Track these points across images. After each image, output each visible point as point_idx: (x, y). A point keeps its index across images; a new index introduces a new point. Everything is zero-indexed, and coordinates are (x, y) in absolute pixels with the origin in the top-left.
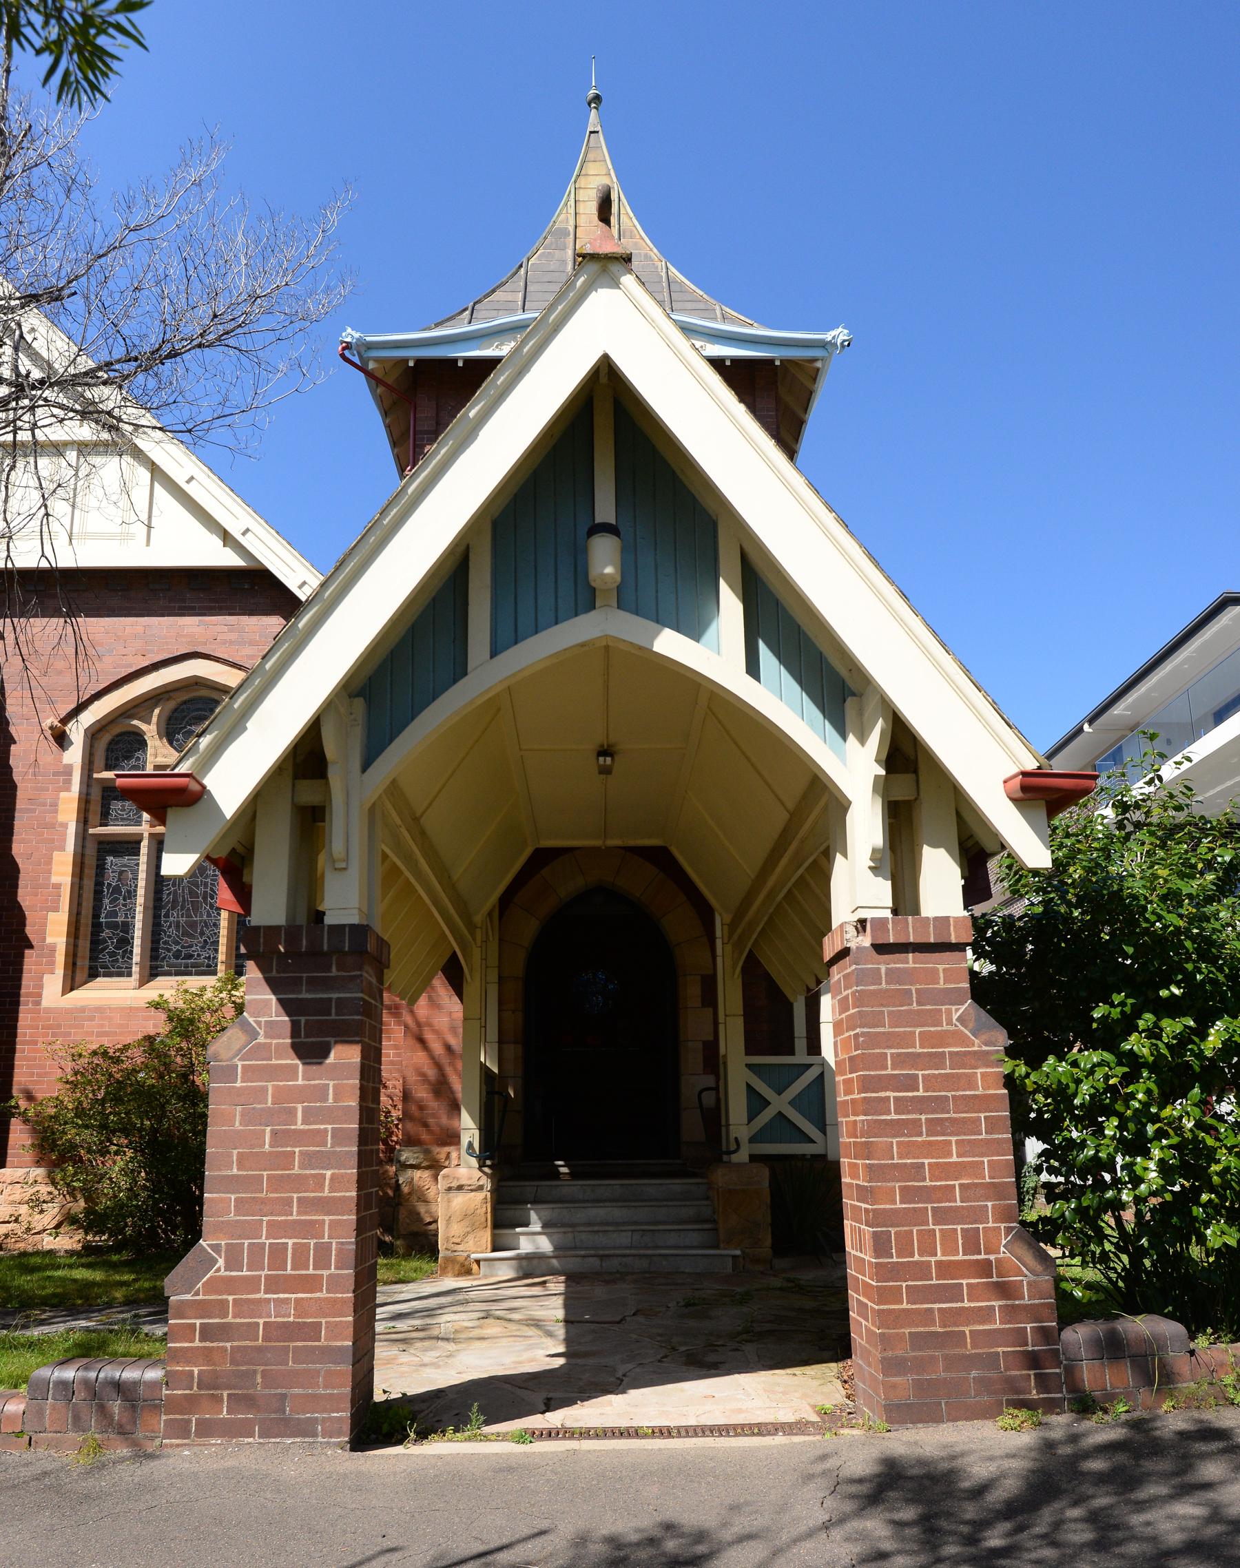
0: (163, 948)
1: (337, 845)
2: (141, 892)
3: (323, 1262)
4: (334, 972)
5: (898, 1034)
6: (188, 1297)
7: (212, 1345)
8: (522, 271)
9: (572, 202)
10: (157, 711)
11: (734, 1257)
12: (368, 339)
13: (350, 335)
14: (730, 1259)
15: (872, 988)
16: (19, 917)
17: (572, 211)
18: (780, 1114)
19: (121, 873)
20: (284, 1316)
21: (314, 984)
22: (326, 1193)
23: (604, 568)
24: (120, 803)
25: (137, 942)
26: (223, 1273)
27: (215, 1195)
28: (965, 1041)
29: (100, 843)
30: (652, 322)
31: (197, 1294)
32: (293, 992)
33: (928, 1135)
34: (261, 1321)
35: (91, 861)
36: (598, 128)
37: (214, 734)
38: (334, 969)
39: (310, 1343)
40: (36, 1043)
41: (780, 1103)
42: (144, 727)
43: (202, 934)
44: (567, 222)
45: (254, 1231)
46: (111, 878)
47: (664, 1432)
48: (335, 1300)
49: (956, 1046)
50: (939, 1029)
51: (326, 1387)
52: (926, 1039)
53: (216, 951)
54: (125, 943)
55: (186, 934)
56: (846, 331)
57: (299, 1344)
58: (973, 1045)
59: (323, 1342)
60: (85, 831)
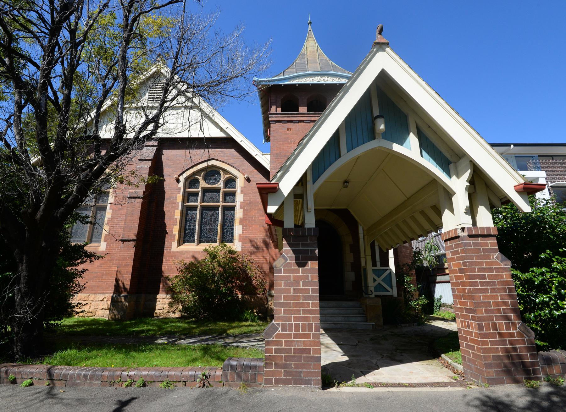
2: (197, 220)
5: (479, 262)
6: (270, 339)
7: (278, 355)
8: (294, 64)
10: (202, 174)
11: (373, 325)
13: (255, 79)
14: (372, 325)
15: (469, 248)
16: (164, 225)
18: (379, 283)
19: (192, 215)
20: (300, 346)
21: (303, 245)
22: (310, 308)
23: (380, 127)
24: (192, 197)
25: (196, 234)
26: (281, 332)
27: (277, 308)
28: (498, 264)
29: (187, 207)
30: (395, 60)
31: (273, 338)
32: (297, 247)
33: (491, 293)
34: (293, 348)
35: (185, 212)
36: (311, 30)
37: (282, 172)
38: (309, 241)
39: (308, 355)
40: (170, 260)
41: (379, 280)
42: (199, 177)
43: (213, 231)
46: (190, 217)
47: (411, 385)
48: (315, 341)
49: (496, 266)
50: (490, 260)
51: (313, 369)
52: (487, 263)
53: (217, 236)
54: (193, 234)
55: (209, 231)
57: (304, 355)
58: (501, 265)
59: (312, 355)
60: (183, 204)
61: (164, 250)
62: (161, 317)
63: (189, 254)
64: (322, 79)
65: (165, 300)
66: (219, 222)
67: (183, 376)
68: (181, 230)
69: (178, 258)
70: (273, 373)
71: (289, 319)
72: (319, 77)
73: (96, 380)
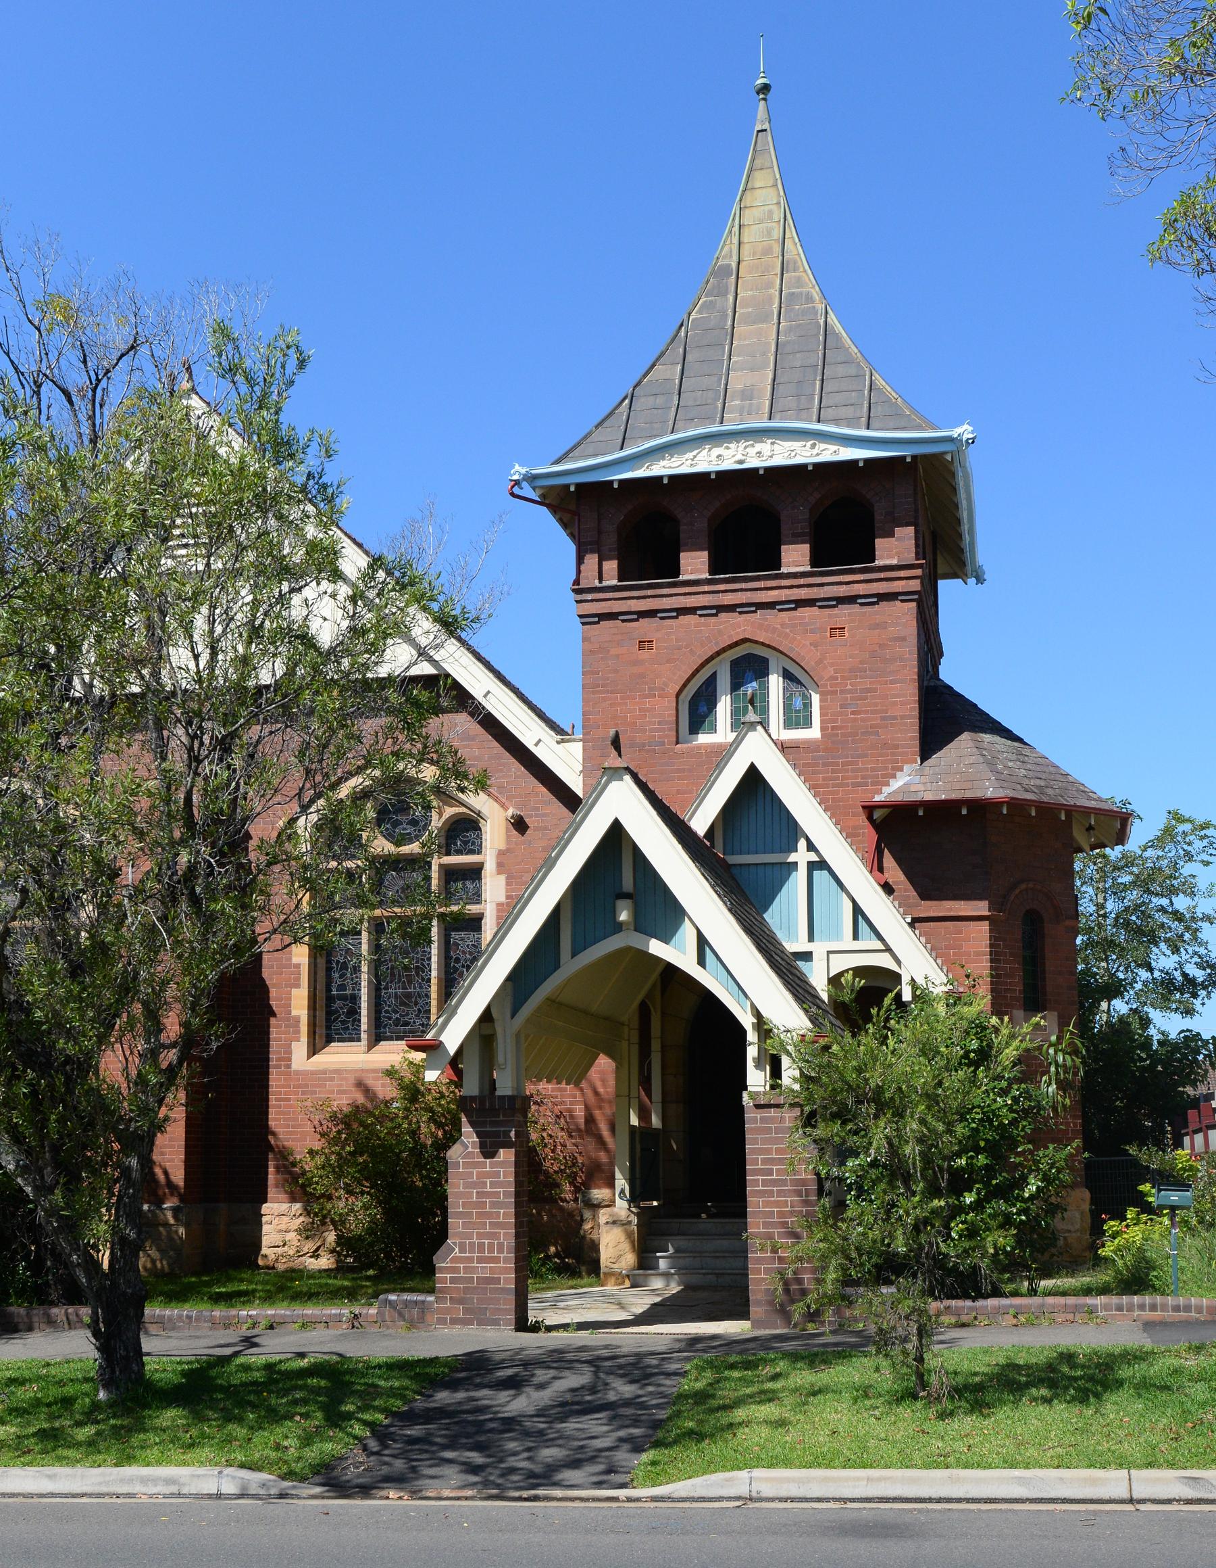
0: (384, 1017)
1: (500, 1058)
3: (500, 1250)
4: (501, 1118)
9: (736, 229)
12: (533, 472)
17: (735, 241)
21: (494, 1124)
25: (364, 1012)
36: (766, 126)
43: (416, 1003)
44: (731, 256)
45: (470, 1236)
54: (354, 1012)
56: (970, 428)
59: (502, 1286)
61: (268, 1067)
62: (281, 1267)
63: (346, 1079)
64: (752, 451)
65: (285, 1219)
66: (434, 973)
67: (324, 1315)
68: (315, 1002)
69: (315, 1093)
70: (447, 1310)
71: (470, 1236)
72: (742, 444)
73: (205, 1321)
